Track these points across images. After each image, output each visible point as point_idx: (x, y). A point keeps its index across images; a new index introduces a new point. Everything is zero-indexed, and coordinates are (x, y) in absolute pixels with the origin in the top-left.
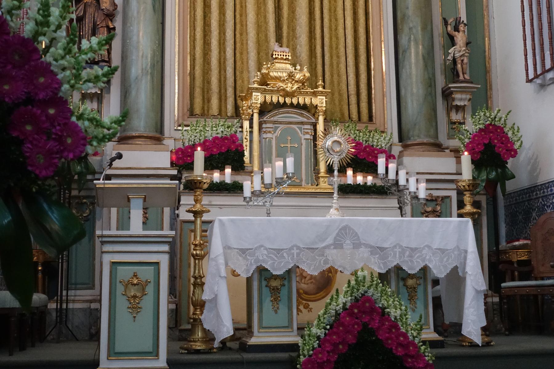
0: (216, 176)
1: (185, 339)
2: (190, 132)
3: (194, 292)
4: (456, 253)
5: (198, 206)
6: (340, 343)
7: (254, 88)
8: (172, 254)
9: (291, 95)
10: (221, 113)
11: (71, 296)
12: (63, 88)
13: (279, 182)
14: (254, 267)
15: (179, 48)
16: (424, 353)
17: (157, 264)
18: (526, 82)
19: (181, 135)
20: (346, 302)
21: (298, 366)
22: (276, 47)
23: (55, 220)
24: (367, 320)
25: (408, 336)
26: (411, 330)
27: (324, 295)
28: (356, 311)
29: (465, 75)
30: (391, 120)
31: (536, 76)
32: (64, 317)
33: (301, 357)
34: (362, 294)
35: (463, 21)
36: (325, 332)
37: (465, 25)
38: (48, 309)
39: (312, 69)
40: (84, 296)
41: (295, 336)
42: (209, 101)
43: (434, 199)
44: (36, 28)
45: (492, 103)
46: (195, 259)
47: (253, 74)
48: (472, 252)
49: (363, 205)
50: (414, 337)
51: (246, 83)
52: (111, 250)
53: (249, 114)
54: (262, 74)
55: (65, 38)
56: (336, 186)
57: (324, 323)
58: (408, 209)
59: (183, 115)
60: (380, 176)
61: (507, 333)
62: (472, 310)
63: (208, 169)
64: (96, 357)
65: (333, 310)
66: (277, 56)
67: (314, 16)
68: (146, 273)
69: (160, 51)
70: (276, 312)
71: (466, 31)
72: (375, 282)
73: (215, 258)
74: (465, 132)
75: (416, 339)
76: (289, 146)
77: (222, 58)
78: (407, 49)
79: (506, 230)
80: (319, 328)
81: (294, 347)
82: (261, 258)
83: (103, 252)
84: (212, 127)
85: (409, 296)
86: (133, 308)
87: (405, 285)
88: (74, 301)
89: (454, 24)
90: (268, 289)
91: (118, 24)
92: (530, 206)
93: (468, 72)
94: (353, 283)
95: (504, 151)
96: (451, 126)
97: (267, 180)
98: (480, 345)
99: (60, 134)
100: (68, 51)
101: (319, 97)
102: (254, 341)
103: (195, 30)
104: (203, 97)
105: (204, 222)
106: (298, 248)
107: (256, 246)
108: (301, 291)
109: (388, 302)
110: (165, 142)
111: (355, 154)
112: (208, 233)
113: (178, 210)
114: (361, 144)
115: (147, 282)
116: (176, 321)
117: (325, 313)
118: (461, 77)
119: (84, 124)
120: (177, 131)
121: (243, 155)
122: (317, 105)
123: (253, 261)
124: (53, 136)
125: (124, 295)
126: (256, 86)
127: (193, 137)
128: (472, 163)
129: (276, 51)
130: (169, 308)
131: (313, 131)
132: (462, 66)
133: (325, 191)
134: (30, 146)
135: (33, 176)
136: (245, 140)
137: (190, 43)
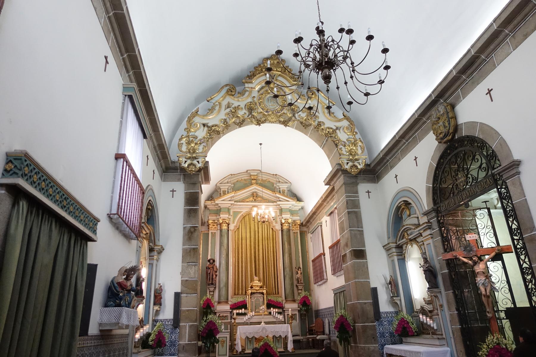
9: (258, 290)
17: (227, 337)
22: (255, 277)
42: (239, 290)
68: (225, 339)
102: (246, 352)
118: (300, 282)
121: (247, 305)
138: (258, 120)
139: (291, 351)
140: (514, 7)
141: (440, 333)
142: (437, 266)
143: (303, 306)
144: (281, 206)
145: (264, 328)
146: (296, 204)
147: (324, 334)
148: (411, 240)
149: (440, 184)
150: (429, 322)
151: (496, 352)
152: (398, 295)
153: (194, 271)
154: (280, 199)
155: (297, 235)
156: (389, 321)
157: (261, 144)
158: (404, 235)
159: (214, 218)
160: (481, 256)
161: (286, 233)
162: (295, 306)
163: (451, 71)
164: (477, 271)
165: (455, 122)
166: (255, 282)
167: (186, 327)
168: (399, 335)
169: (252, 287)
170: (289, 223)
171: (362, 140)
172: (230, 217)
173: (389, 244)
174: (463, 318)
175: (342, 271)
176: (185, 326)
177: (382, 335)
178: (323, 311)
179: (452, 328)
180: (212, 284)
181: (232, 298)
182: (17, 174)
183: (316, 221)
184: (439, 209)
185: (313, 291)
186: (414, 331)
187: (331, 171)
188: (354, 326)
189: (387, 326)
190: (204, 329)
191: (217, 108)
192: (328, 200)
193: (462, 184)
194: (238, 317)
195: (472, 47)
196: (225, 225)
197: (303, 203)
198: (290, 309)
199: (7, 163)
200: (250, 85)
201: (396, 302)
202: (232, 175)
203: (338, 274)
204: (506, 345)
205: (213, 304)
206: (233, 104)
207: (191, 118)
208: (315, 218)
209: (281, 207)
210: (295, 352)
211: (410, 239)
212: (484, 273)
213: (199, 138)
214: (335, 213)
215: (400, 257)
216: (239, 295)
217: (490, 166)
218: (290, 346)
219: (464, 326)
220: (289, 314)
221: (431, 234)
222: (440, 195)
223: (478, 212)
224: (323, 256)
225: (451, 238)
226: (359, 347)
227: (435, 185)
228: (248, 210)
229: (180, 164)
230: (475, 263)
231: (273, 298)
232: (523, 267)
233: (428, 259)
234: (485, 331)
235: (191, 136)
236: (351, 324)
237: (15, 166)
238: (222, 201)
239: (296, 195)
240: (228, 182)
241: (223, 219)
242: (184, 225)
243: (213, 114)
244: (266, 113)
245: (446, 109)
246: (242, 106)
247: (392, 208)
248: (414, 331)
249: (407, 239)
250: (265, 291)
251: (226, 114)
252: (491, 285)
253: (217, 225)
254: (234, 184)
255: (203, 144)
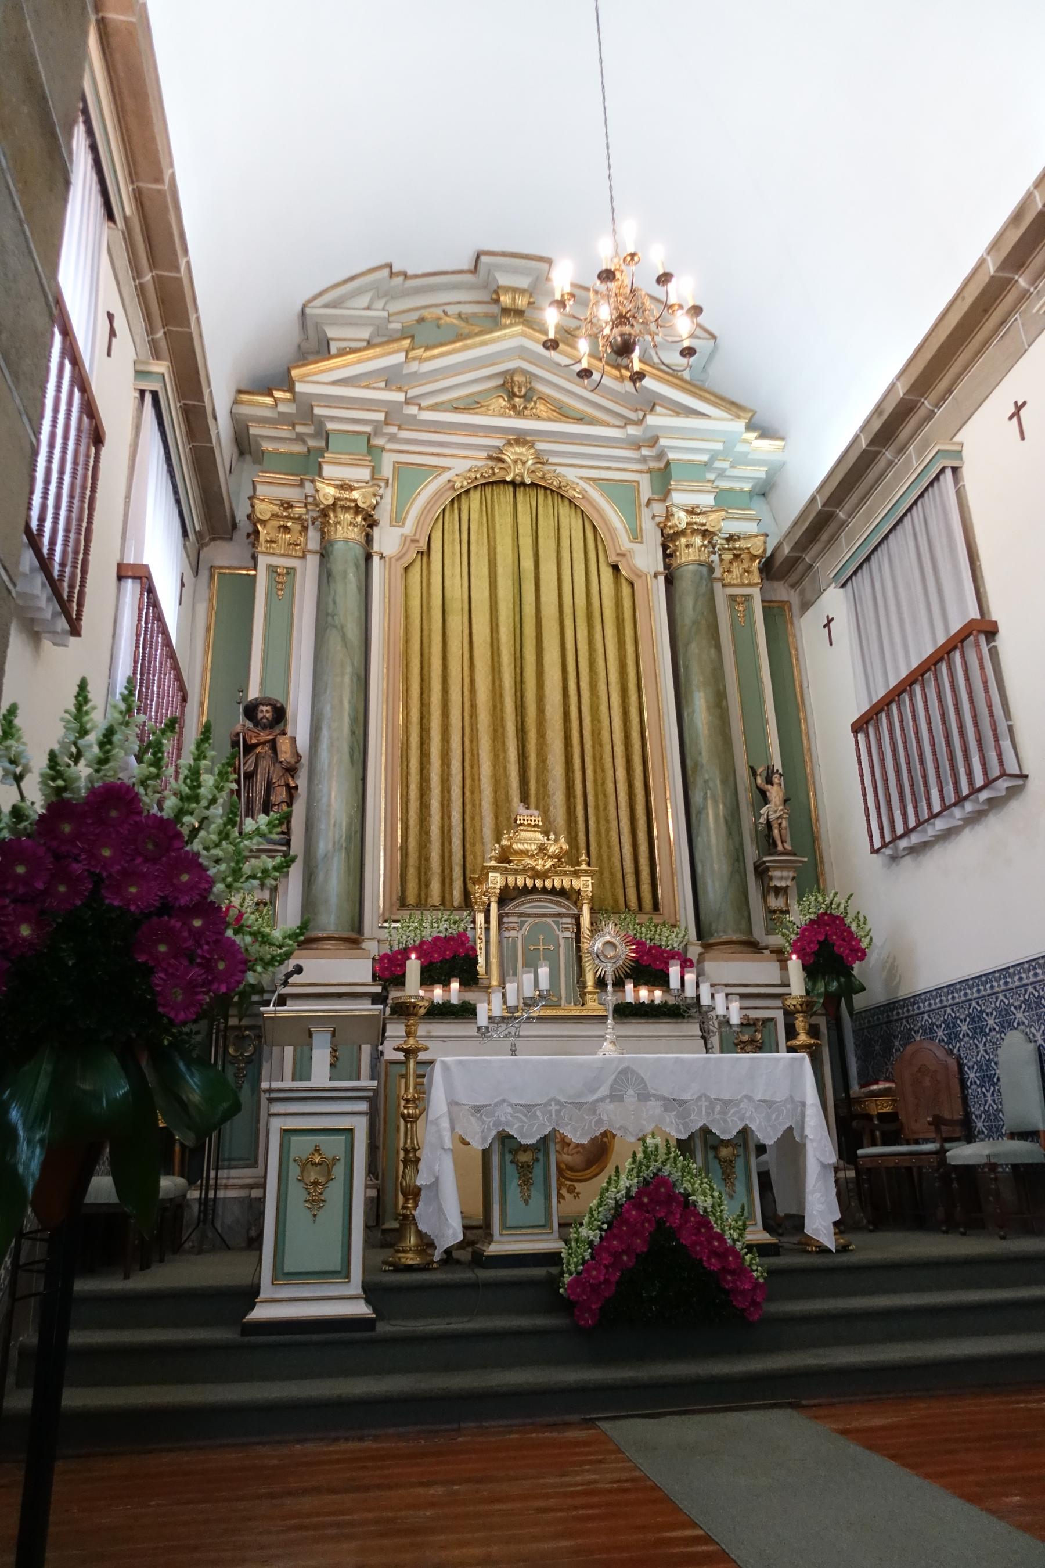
0: (438, 993)
1: (390, 1245)
2: (400, 930)
3: (404, 1172)
4: (789, 1106)
5: (411, 1041)
6: (624, 1252)
7: (490, 867)
8: (373, 1115)
9: (544, 875)
11: (223, 1178)
12: (215, 889)
13: (529, 1003)
14: (494, 1133)
15: (386, 813)
16: (750, 1266)
17: (351, 1131)
18: (871, 853)
19: (387, 935)
20: (631, 1186)
21: (561, 1290)
22: (521, 809)
23: (195, 1087)
24: (663, 1214)
25: (725, 1239)
26: (730, 1229)
27: (597, 1170)
28: (646, 1200)
29: (785, 845)
30: (685, 908)
31: (885, 845)
32: (211, 1212)
33: (566, 1275)
34: (653, 1173)
35: (777, 771)
36: (601, 1235)
37: (781, 775)
38: (188, 1200)
39: (571, 838)
40: (242, 1178)
41: (555, 1241)
42: (427, 885)
43: (752, 1022)
44: (180, 804)
45: (825, 884)
46: (406, 1122)
47: (489, 846)
48: (813, 1105)
49: (650, 1034)
50: (734, 1241)
51: (479, 859)
52: (282, 1111)
53: (484, 903)
54: (502, 847)
55: (221, 818)
56: (611, 1008)
57: (599, 1221)
58: (715, 1040)
59: (392, 905)
60: (672, 991)
61: (871, 1227)
62: (817, 1195)
63: (426, 984)
64: (256, 1280)
65: (611, 1199)
66: (522, 822)
67: (573, 765)
68: (333, 1146)
69: (359, 816)
70: (526, 1202)
71: (782, 783)
72: (672, 1155)
73: (436, 1119)
74: (790, 925)
75: (737, 1243)
76: (541, 948)
77: (446, 851)
78: (703, 809)
79: (858, 1067)
80: (591, 1229)
81: (552, 1259)
82: (503, 1119)
83: (270, 1115)
84: (432, 923)
85: (723, 1174)
86: (313, 1201)
87: (716, 1157)
88: (226, 1187)
89: (765, 774)
90: (514, 1166)
91: (301, 781)
93: (788, 839)
94: (640, 1156)
95: (847, 951)
96: (769, 916)
97: (512, 1001)
98: (834, 1251)
99: (208, 956)
100: (224, 835)
101: (582, 878)
102: (493, 1249)
103: (407, 787)
104: (420, 880)
105: (419, 1063)
106: (558, 1102)
107: (496, 1100)
108: (563, 1166)
109: (693, 1185)
110: (364, 945)
111: (635, 960)
112: (425, 1080)
113: (382, 1044)
114: (643, 944)
115: (335, 1160)
116: (378, 1216)
117: (600, 1205)
118: (780, 848)
119: (244, 941)
120: (381, 930)
121: (477, 963)
122: (579, 890)
123: (491, 1124)
124: (198, 960)
125: (299, 1180)
126: (493, 863)
127: (404, 937)
128: (804, 969)
129: (520, 815)
130: (367, 1195)
131: (575, 926)
132: (780, 831)
133: (595, 1014)
134: (162, 975)
135: (165, 1020)
136: (478, 941)
137: (401, 806)
155: (749, 612)
228: (480, 463)
238: (334, 383)
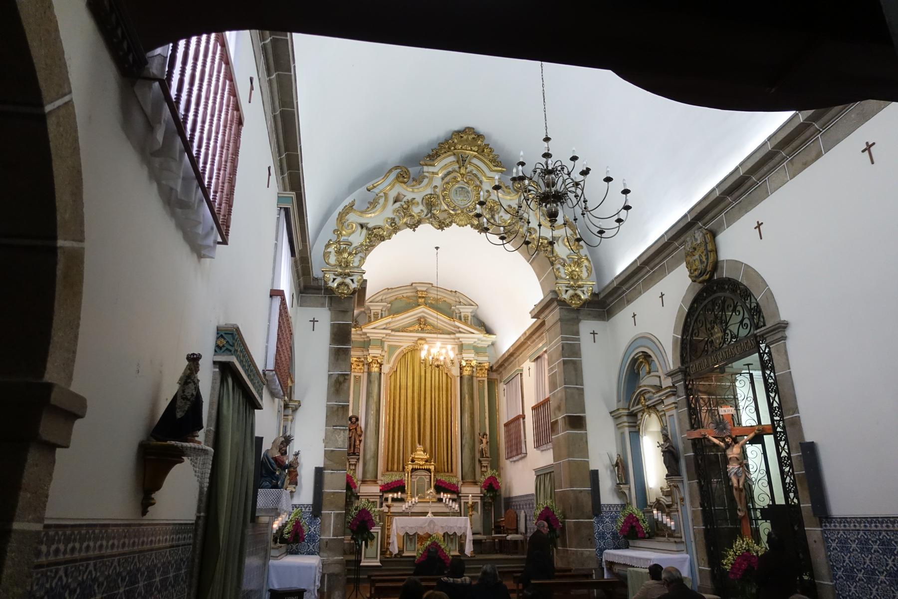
9: (422, 465)
10: (398, 470)
22: (418, 446)
42: (394, 464)
81: (414, 557)
92: (96, 574)
102: (404, 555)
121: (405, 487)
138: (440, 222)
139: (469, 555)
140: (792, 129)
141: (679, 535)
142: (681, 446)
143: (487, 492)
144: (461, 340)
145: (431, 521)
146: (484, 338)
147: (517, 533)
148: (649, 407)
149: (692, 336)
150: (666, 520)
151: (744, 561)
152: (627, 482)
153: (342, 439)
154: (460, 330)
156: (612, 517)
157: (437, 248)
158: (640, 400)
159: (359, 353)
160: (736, 436)
161: (467, 381)
162: (477, 490)
163: (713, 190)
164: (729, 457)
165: (716, 256)
166: (418, 453)
167: (331, 516)
168: (625, 537)
169: (413, 461)
170: (472, 367)
171: (589, 258)
172: (383, 354)
173: (618, 410)
174: (708, 516)
175: (550, 444)
176: (330, 515)
177: (602, 536)
178: (518, 499)
179: (694, 529)
180: (354, 454)
181: (383, 475)
182: (230, 351)
183: (515, 367)
184: (688, 370)
185: (502, 469)
186: (645, 532)
187: (542, 300)
188: (563, 523)
189: (609, 525)
190: (355, 519)
191: (382, 201)
192: (534, 337)
193: (718, 341)
194: (396, 504)
195: (741, 164)
196: (375, 365)
197: (494, 336)
198: (470, 495)
199: (218, 338)
200: (431, 169)
201: (625, 491)
202: (388, 289)
203: (544, 447)
204: (757, 552)
205: (354, 483)
206: (405, 196)
207: (344, 215)
208: (512, 362)
209: (461, 342)
210: (475, 556)
211: (647, 405)
212: (737, 459)
213: (354, 246)
214: (544, 358)
215: (633, 429)
216: (393, 471)
217: (753, 324)
218: (469, 549)
219: (709, 527)
220: (467, 503)
221: (674, 403)
222: (690, 351)
223: (739, 378)
224: (521, 420)
225: (700, 410)
226: (569, 552)
227: (685, 337)
228: (410, 344)
229: (326, 283)
230: (728, 446)
231: (443, 477)
232: (782, 456)
233: (670, 437)
234: (736, 533)
235: (342, 241)
236: (560, 520)
237: (227, 342)
238: (374, 328)
239: (484, 323)
240: (382, 301)
241: (374, 357)
242: (329, 371)
243: (375, 209)
244: (452, 212)
245: (705, 237)
246: (419, 199)
247: (626, 358)
248: (645, 532)
249: (643, 405)
250: (432, 468)
251: (394, 211)
252: (746, 476)
253: (363, 365)
254: (390, 303)
255: (360, 255)
